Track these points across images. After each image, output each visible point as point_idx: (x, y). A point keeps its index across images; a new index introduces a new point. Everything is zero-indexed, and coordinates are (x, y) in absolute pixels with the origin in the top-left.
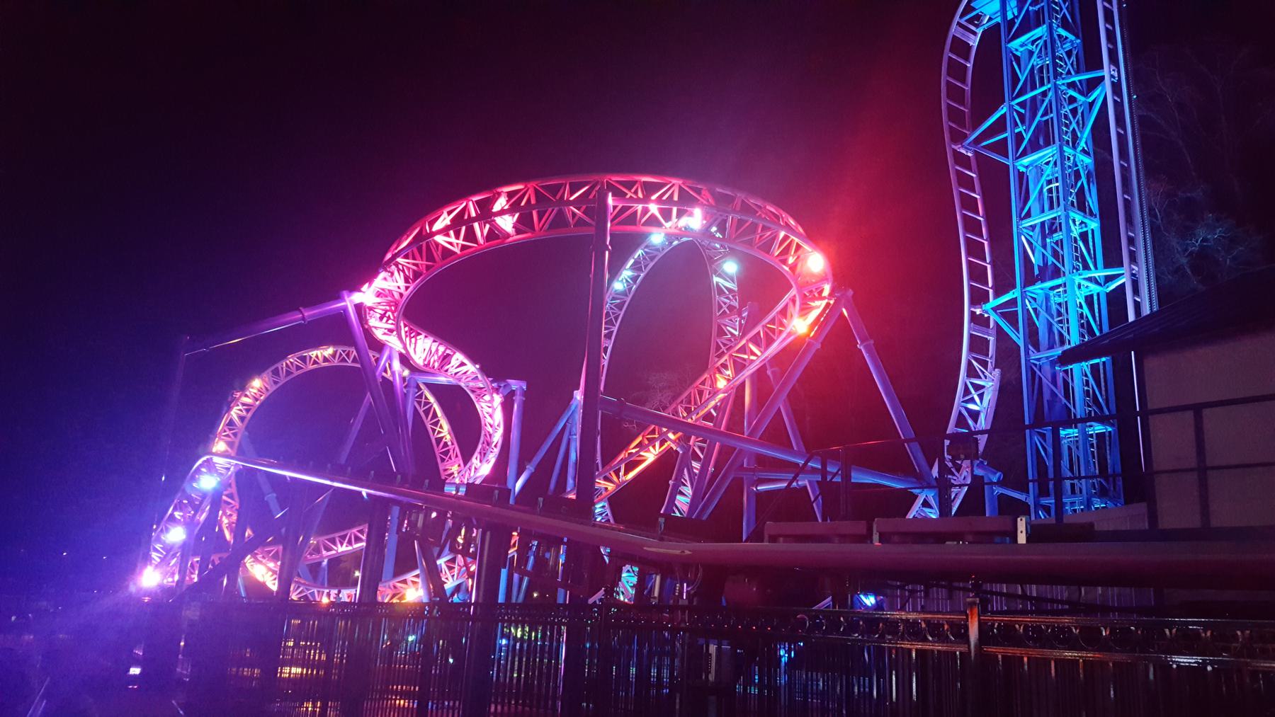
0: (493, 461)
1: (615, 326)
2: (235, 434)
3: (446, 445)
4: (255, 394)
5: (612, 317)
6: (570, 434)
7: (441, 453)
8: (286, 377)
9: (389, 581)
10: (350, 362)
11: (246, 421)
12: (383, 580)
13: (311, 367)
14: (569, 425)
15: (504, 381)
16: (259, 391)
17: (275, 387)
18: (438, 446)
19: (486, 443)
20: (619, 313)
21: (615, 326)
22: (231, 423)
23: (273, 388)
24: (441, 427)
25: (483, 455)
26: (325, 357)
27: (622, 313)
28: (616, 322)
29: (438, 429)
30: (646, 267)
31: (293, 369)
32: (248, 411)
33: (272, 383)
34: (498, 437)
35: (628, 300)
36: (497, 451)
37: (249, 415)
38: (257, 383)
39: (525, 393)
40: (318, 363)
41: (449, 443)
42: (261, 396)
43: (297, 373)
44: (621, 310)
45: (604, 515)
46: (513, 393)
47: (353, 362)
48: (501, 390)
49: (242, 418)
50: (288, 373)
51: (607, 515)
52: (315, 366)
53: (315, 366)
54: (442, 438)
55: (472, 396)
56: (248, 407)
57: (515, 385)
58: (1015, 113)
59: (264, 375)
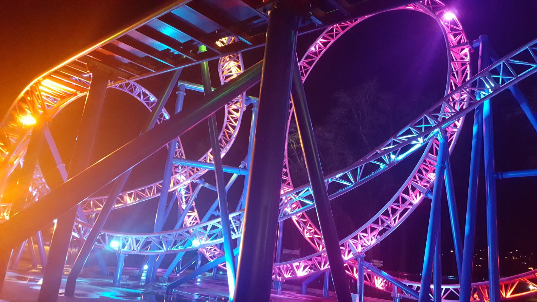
27: (311, 68)
30: (336, 35)
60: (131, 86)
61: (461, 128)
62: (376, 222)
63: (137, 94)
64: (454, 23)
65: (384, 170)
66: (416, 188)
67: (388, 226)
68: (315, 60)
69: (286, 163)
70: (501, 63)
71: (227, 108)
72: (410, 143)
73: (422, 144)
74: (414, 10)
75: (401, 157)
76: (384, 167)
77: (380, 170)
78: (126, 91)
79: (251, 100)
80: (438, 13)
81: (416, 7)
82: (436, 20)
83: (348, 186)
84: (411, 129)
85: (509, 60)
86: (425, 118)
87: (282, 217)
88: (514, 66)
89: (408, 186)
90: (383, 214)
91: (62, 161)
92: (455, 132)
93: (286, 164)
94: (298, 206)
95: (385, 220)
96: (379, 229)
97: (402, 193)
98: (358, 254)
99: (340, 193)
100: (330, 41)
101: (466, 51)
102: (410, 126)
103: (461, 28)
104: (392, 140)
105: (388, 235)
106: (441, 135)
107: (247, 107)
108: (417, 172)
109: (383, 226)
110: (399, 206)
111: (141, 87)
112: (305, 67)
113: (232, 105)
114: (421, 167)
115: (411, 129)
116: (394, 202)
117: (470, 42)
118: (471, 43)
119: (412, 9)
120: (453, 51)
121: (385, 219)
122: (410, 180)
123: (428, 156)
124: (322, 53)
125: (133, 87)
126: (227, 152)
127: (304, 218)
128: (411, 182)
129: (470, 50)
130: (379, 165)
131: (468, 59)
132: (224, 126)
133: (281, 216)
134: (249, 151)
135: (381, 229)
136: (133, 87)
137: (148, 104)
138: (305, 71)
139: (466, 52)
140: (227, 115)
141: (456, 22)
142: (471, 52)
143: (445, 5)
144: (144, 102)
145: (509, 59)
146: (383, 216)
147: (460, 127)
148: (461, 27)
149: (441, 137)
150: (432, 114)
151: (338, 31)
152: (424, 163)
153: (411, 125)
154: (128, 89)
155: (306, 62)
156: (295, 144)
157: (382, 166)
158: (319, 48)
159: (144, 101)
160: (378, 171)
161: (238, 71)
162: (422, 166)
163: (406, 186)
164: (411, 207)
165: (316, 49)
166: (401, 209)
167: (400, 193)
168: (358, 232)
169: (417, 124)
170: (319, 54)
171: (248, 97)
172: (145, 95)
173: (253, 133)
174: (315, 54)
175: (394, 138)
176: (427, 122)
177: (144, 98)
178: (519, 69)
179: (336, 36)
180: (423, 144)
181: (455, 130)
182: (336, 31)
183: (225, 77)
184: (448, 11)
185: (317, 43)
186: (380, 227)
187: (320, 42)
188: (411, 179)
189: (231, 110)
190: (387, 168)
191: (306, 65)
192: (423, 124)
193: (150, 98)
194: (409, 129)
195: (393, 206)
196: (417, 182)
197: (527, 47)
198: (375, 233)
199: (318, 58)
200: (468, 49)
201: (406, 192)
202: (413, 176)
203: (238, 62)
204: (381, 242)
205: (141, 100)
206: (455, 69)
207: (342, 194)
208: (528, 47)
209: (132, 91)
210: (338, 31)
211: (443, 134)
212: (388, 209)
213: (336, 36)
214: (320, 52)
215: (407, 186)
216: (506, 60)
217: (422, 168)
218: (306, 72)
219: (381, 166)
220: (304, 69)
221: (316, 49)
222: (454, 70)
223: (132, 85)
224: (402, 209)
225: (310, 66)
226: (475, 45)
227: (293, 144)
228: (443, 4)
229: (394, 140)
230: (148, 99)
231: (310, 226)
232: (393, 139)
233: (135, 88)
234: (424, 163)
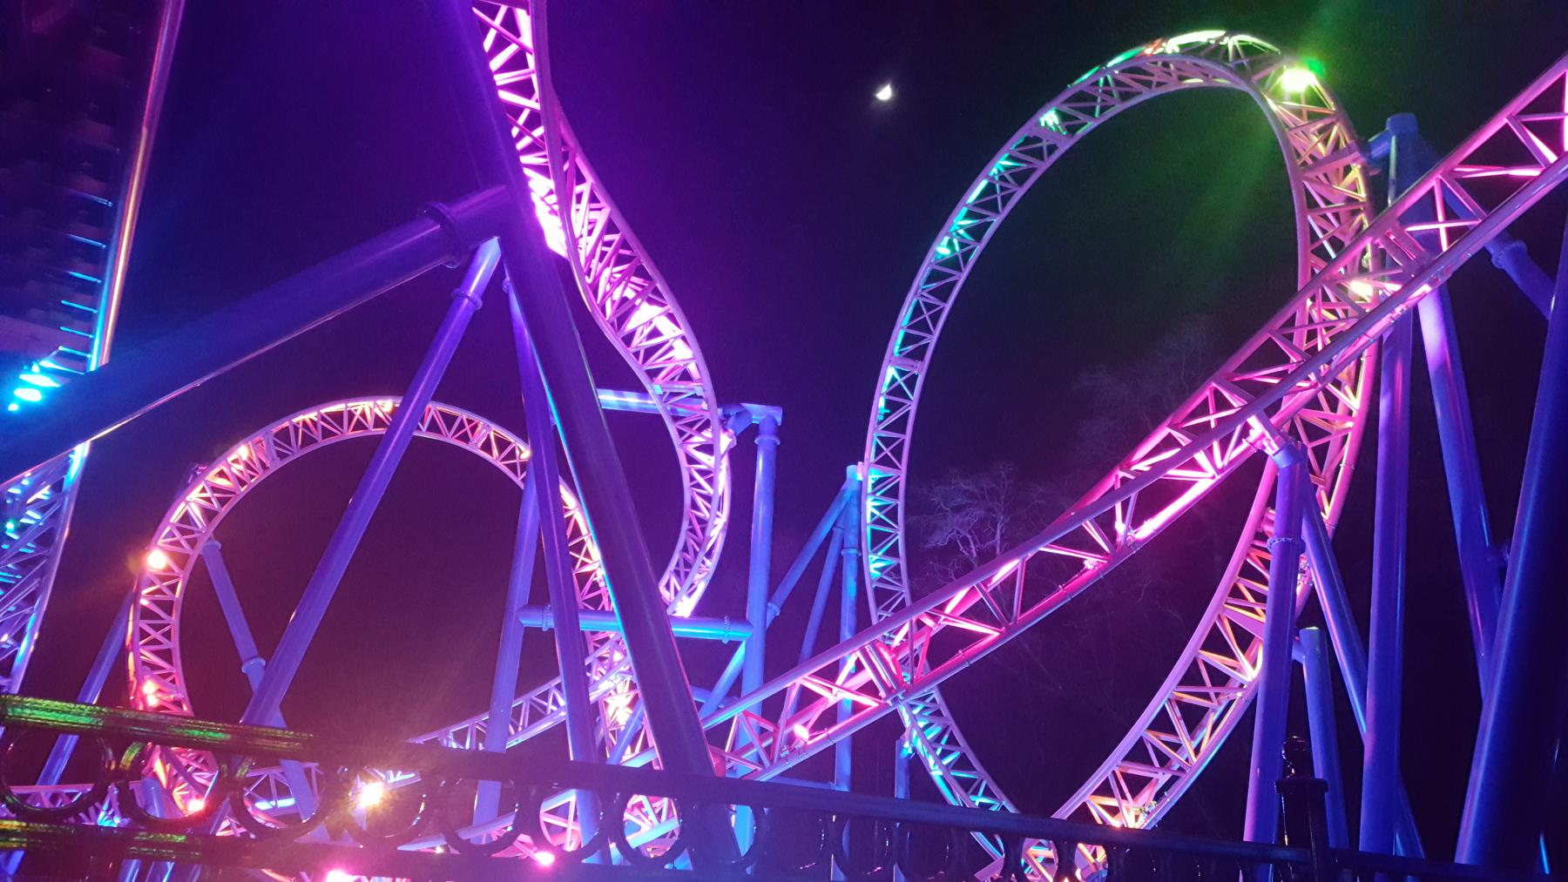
0: (701, 587)
1: (931, 333)
2: (192, 543)
3: (595, 586)
4: (241, 472)
5: (926, 315)
6: (842, 547)
7: (585, 601)
8: (302, 447)
9: (492, 822)
10: (424, 429)
11: (217, 521)
12: (474, 824)
13: (350, 434)
14: (838, 531)
15: (738, 404)
16: (248, 466)
17: (279, 464)
18: (582, 587)
19: (682, 575)
20: (942, 304)
21: (931, 333)
22: (186, 518)
23: (275, 465)
24: (588, 555)
25: (683, 572)
26: (377, 417)
27: (948, 306)
28: (935, 325)
29: (581, 558)
30: (1005, 200)
31: (318, 435)
32: (222, 502)
33: (275, 454)
34: (717, 532)
35: (962, 278)
36: (711, 564)
37: (224, 511)
38: (243, 451)
39: (780, 431)
40: (365, 428)
41: (602, 585)
42: (252, 477)
43: (323, 443)
44: (1020, 184)
45: (928, 700)
46: (753, 430)
47: (429, 430)
48: (731, 421)
49: (209, 514)
50: (307, 440)
51: (934, 701)
52: (359, 433)
53: (359, 433)
54: (589, 574)
55: (672, 429)
56: (223, 495)
57: (758, 412)
58: (1320, 290)
59: (259, 436)
60: (462, 426)
61: (1364, 416)
62: (1139, 753)
63: (480, 445)
64: (1315, 99)
65: (1096, 574)
66: (1253, 636)
67: (1181, 769)
68: (955, 283)
69: (903, 595)
70: (1433, 183)
71: (681, 445)
72: (1161, 477)
73: (1213, 477)
74: (1206, 85)
75: (1149, 528)
76: (1096, 563)
77: (1085, 575)
78: (450, 439)
79: (751, 415)
80: (1256, 78)
81: (1207, 75)
82: (1248, 94)
83: (984, 636)
84: (1176, 434)
85: (1457, 169)
86: (1216, 393)
87: (786, 759)
88: (1472, 186)
89: (1218, 624)
90: (1152, 727)
91: (255, 652)
92: (1349, 429)
93: (904, 599)
94: (949, 732)
95: (1161, 744)
96: (1158, 780)
97: (1201, 649)
98: (1093, 869)
99: (961, 663)
100: (988, 220)
101: (1356, 173)
102: (1170, 426)
103: (1334, 109)
104: (1117, 476)
105: (1181, 795)
106: (1273, 443)
107: (739, 438)
108: (1239, 575)
109: (1169, 769)
110: (1206, 696)
111: (488, 423)
112: (929, 307)
113: (691, 436)
114: (1248, 555)
115: (1176, 434)
116: (1182, 683)
117: (1358, 143)
118: (1364, 148)
119: (1200, 83)
120: (1309, 180)
121: (1164, 742)
122: (1219, 604)
123: (1267, 518)
124: (973, 258)
125: (467, 428)
126: (709, 578)
127: (970, 768)
128: (1224, 610)
129: (1364, 171)
130: (1082, 560)
131: (1362, 194)
132: (687, 501)
133: (783, 755)
134: (752, 561)
135: (1162, 778)
136: (467, 428)
137: (513, 467)
138: (930, 316)
139: (1356, 176)
140: (687, 466)
141: (1320, 99)
142: (1371, 174)
143: (1281, 50)
144: (501, 465)
145: (1456, 167)
146: (1154, 732)
147: (1359, 411)
148: (1332, 106)
149: (1277, 448)
150: (1237, 379)
151: (1008, 189)
152: (1258, 543)
153: (1172, 419)
154: (454, 435)
155: (928, 290)
156: (975, 543)
157: (1091, 562)
158: (962, 245)
159: (501, 461)
160: (1077, 580)
161: (674, 331)
162: (1252, 554)
163: (1212, 625)
164: (1239, 694)
165: (953, 250)
166: (1215, 704)
167: (1195, 650)
168: (1084, 795)
169: (1194, 415)
170: (966, 262)
171: (742, 407)
172: (503, 444)
173: (762, 511)
174: (954, 263)
175: (1122, 470)
176: (1222, 404)
177: (500, 452)
178: (1491, 195)
179: (1004, 205)
180: (1218, 477)
181: (1350, 424)
182: (1002, 189)
183: (645, 354)
184: (1290, 65)
185: (952, 230)
186: (1160, 773)
187: (961, 227)
188: (1221, 599)
189: (691, 449)
190: (1105, 567)
191: (933, 300)
192: (1211, 412)
193: (517, 452)
194: (1170, 434)
195: (1182, 698)
196: (1253, 611)
197: (1506, 121)
198: (1147, 795)
199: (964, 276)
200: (1359, 166)
201: (1215, 643)
202: (1226, 589)
203: (663, 305)
204: (1159, 823)
205: (495, 458)
206: (1324, 232)
207: (967, 665)
208: (1508, 118)
209: (465, 438)
210: (1008, 189)
211: (1278, 437)
212: (1164, 706)
213: (1004, 205)
214: (966, 256)
215: (1215, 624)
216: (1445, 170)
217: (1254, 561)
218: (935, 321)
219: (1085, 562)
220: (928, 310)
221: (953, 250)
222: (1320, 235)
223: (462, 421)
224: (1220, 704)
225: (945, 300)
226: (1376, 152)
227: (965, 542)
228: (1276, 49)
229: (1124, 477)
230: (512, 455)
231: (988, 793)
232: (1121, 474)
233: (473, 429)
234: (1258, 543)
